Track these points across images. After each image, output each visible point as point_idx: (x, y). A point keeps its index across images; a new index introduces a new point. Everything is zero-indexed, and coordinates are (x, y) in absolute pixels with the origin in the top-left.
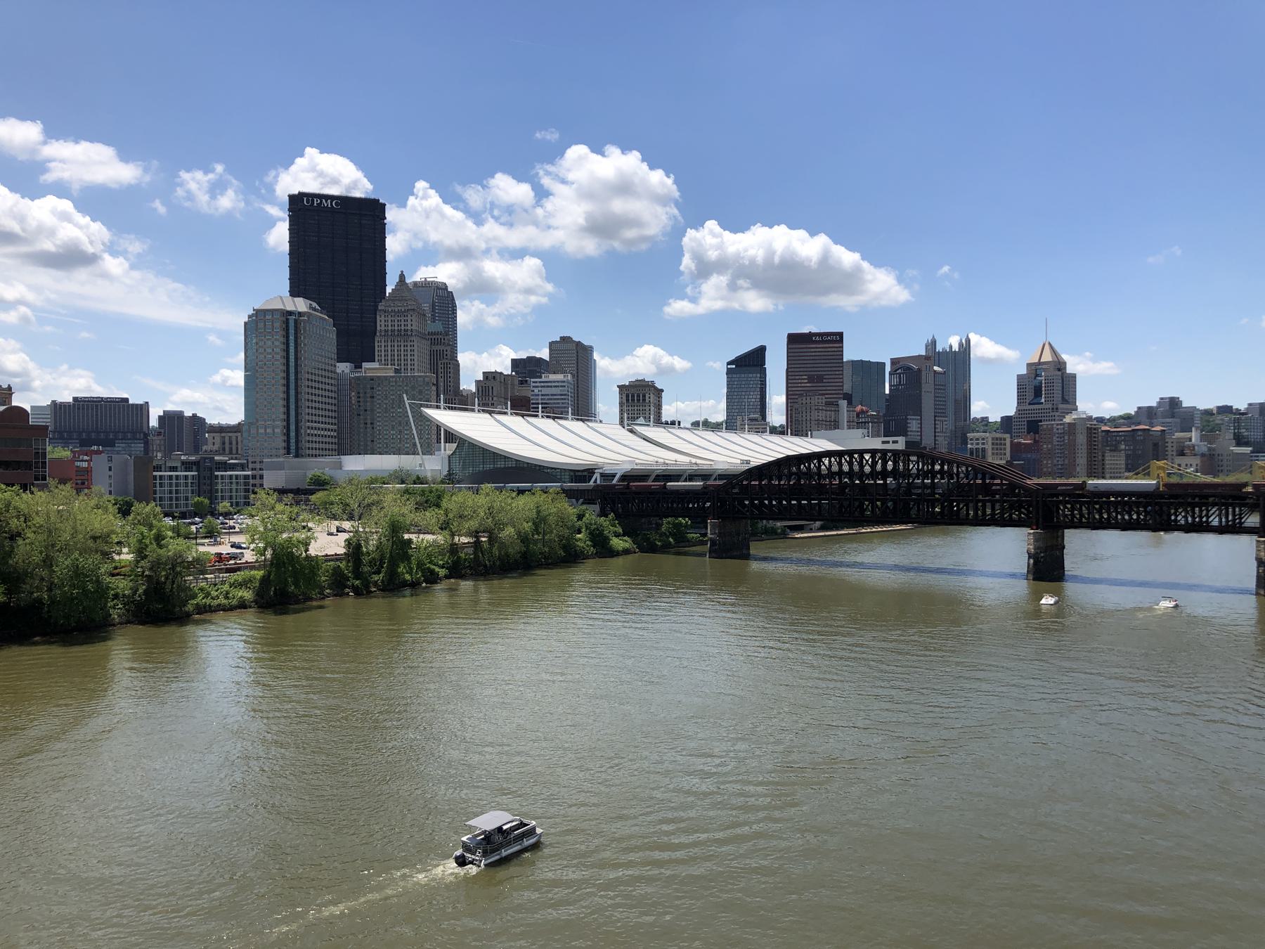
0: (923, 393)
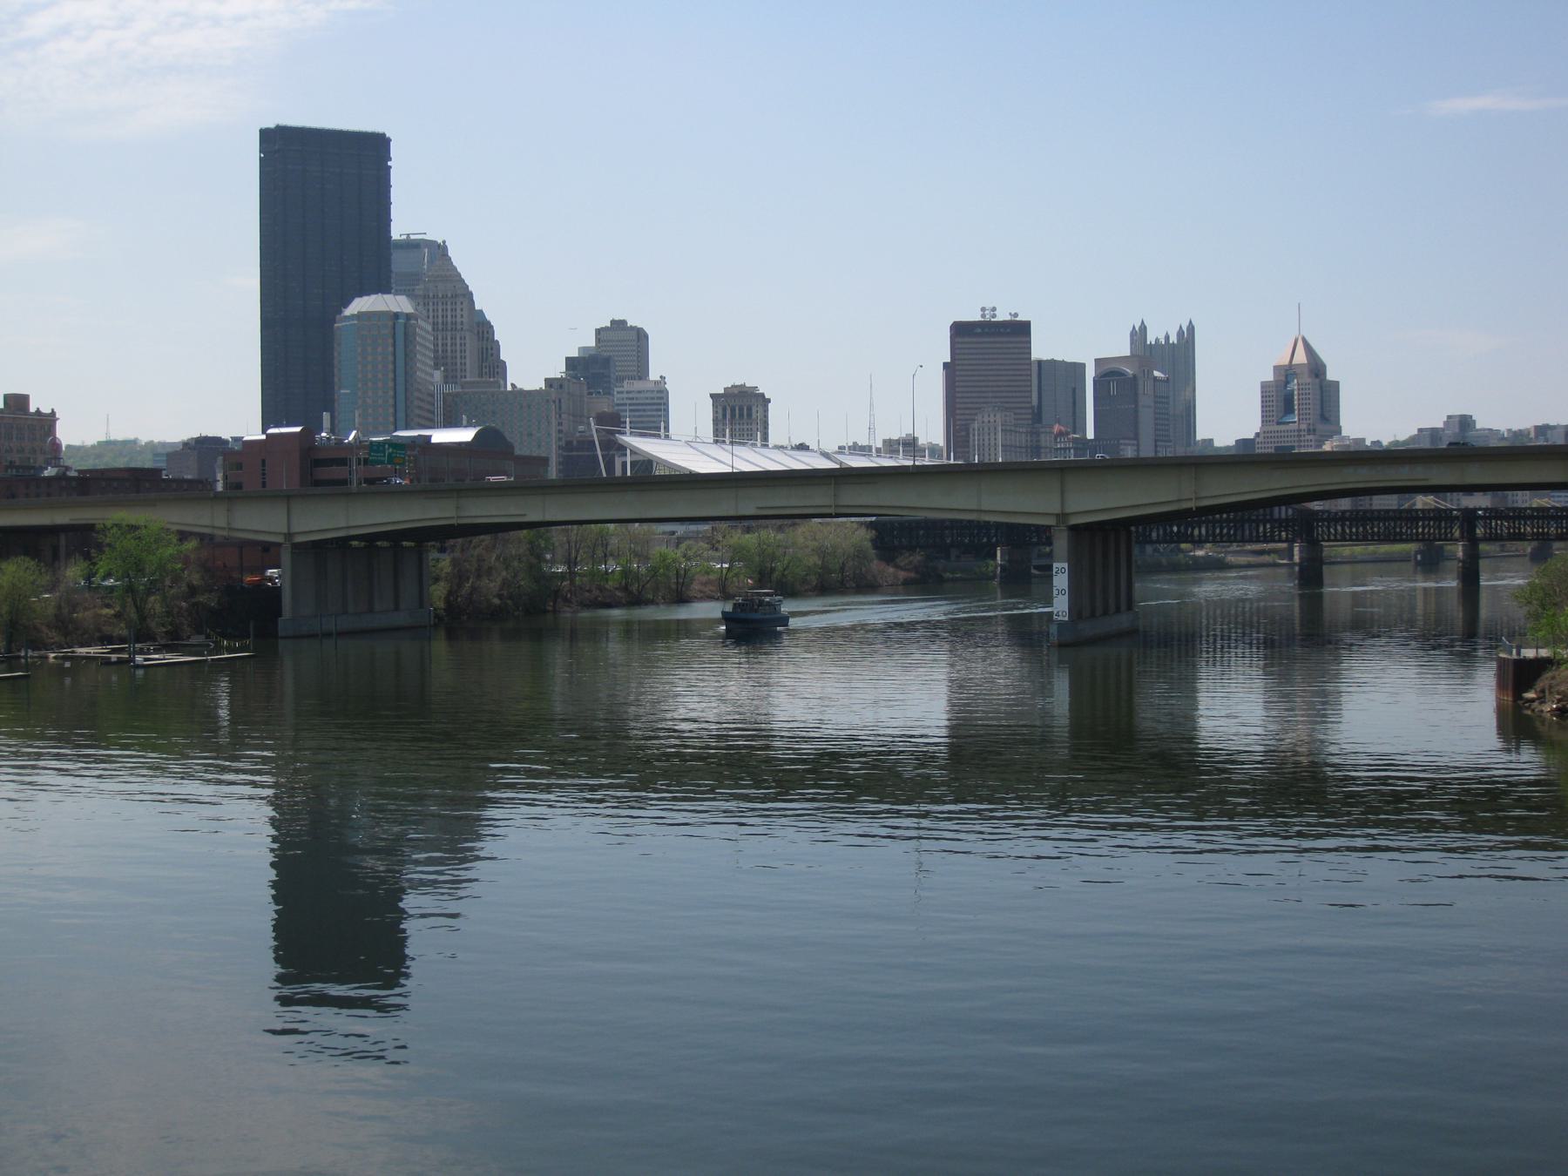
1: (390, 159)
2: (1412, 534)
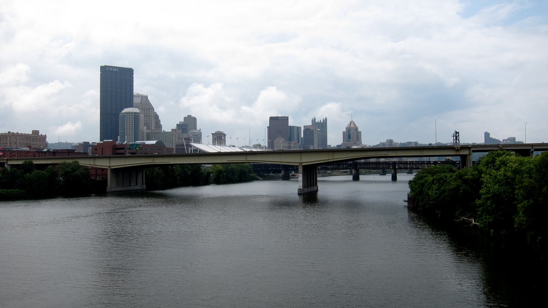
0: (314, 138)
1: (133, 75)
2: (377, 167)
